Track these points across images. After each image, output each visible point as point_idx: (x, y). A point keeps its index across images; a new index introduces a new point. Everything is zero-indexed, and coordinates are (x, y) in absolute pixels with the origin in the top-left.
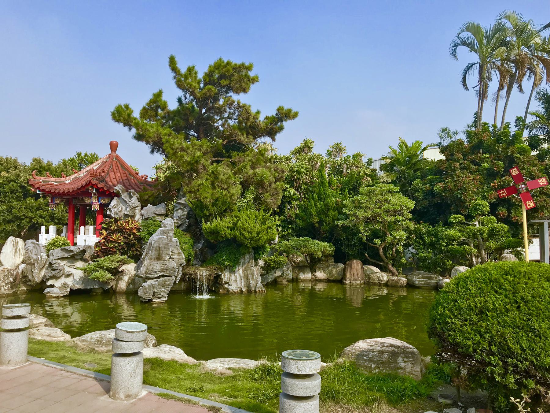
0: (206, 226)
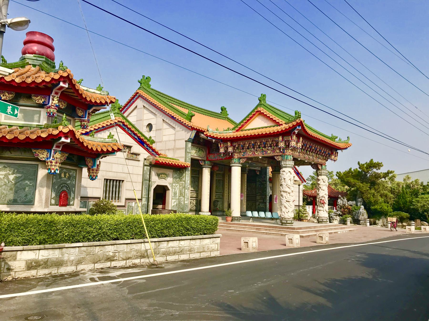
0: (373, 208)
